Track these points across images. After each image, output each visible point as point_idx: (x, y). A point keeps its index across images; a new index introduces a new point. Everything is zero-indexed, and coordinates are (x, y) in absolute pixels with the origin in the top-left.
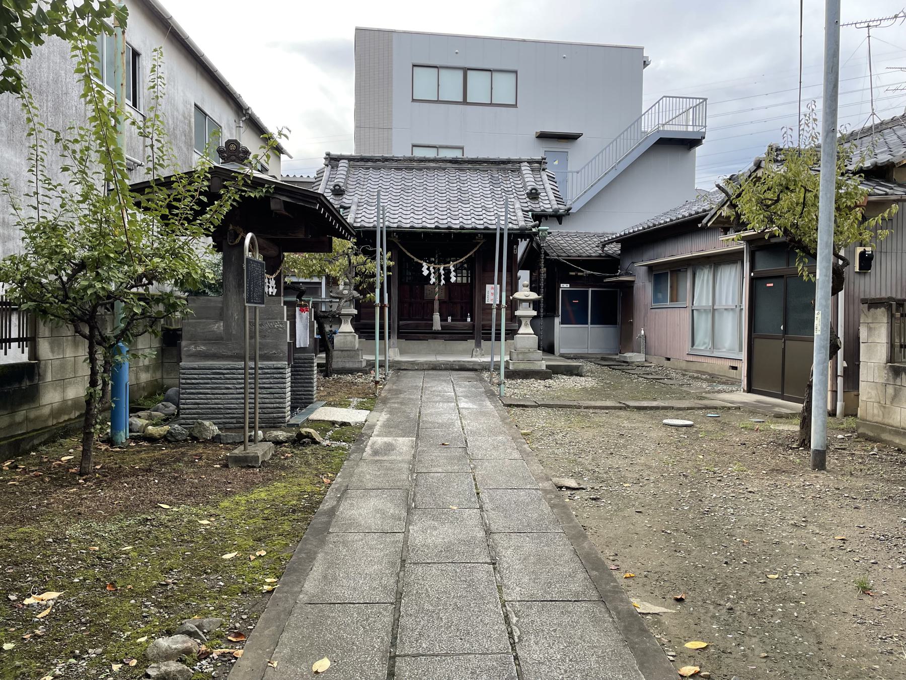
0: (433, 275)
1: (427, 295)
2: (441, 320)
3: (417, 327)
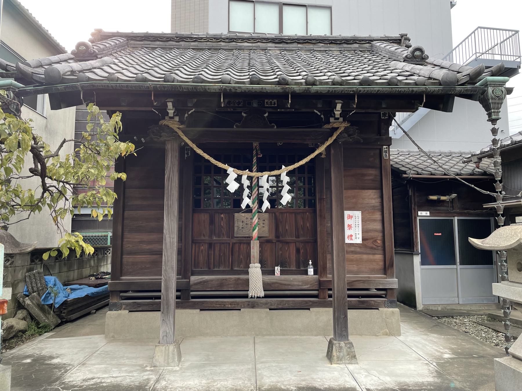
0: (247, 191)
2: (264, 273)
3: (221, 285)
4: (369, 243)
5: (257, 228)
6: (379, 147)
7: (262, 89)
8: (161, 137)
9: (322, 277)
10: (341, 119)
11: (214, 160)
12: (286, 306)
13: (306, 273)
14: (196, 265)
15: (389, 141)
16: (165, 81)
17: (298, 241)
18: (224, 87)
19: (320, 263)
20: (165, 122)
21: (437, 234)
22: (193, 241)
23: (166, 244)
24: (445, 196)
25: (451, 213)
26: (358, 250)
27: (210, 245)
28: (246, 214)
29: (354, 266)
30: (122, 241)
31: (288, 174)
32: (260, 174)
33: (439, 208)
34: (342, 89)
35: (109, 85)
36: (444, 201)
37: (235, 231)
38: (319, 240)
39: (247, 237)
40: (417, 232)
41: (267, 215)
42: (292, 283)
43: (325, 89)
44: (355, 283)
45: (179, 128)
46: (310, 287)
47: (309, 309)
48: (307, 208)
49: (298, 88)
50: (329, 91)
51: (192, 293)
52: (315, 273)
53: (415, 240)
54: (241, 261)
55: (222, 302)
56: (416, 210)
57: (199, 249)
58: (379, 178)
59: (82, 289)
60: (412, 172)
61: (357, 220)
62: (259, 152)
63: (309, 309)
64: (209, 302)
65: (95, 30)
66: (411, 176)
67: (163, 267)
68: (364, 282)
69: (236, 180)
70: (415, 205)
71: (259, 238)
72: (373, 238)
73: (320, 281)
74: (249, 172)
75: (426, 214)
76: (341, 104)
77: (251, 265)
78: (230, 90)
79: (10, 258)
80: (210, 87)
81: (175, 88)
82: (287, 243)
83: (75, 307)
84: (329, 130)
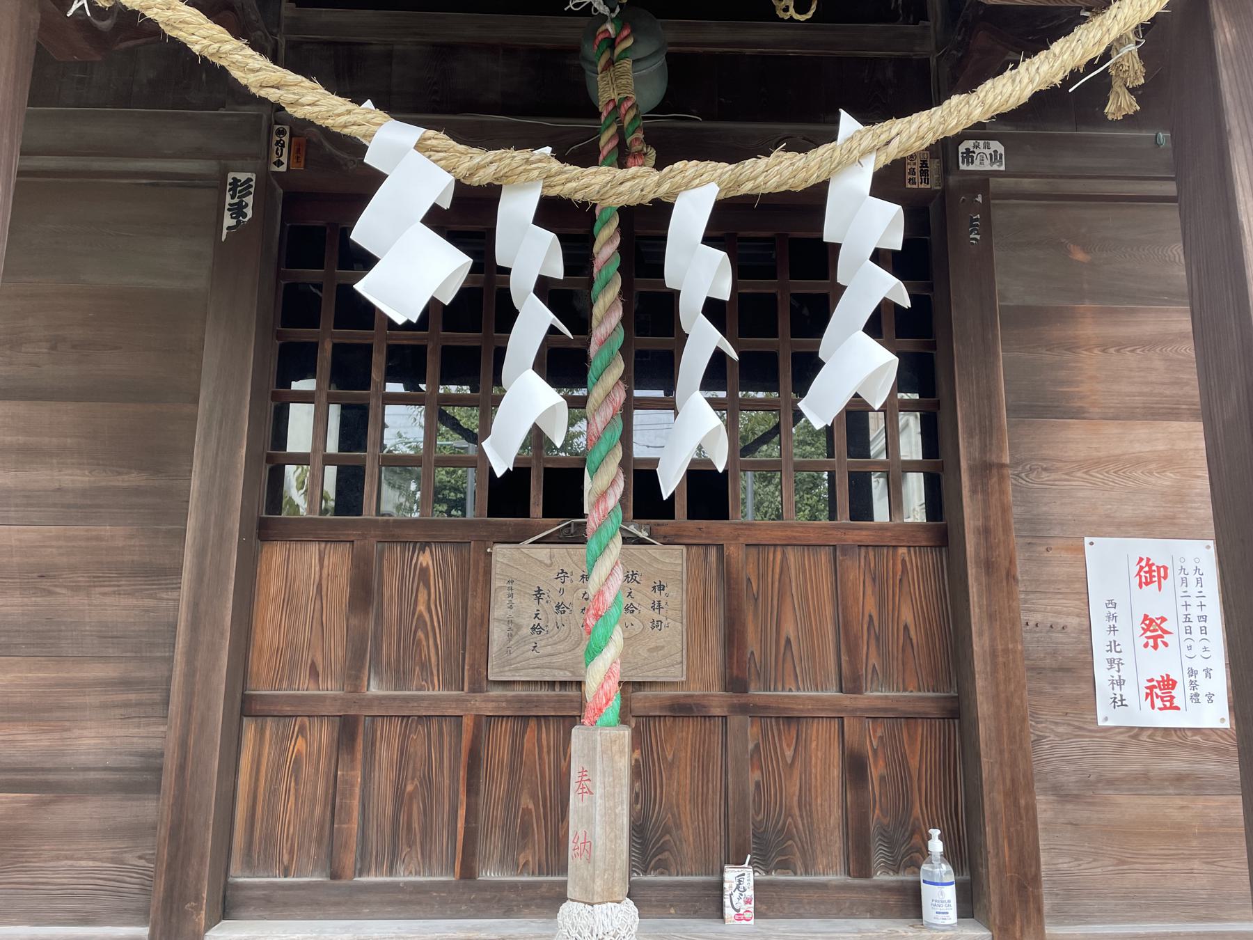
0: (534, 322)
17: (856, 713)
22: (246, 706)
27: (348, 730)
28: (559, 551)
29: (1196, 864)
37: (494, 649)
38: (984, 708)
39: (563, 684)
54: (526, 832)
61: (1193, 589)
69: (435, 219)
74: (556, 165)
82: (791, 720)
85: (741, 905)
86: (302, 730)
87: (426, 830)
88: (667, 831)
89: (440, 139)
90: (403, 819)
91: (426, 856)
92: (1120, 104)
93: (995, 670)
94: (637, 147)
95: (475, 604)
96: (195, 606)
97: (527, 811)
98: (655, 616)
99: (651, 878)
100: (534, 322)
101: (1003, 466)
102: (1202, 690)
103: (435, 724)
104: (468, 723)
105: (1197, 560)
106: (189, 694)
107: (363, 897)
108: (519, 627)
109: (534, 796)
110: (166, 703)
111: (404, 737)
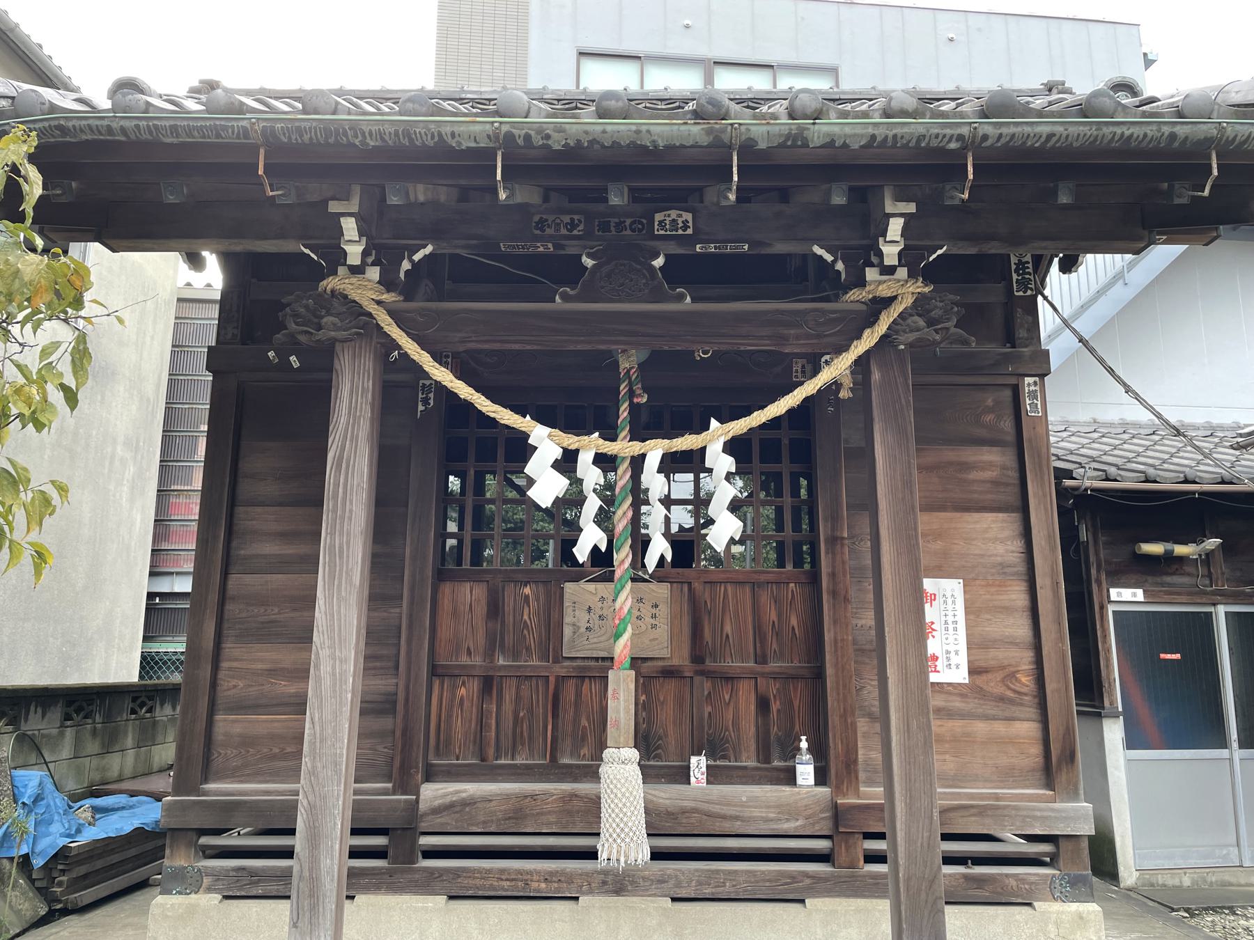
0: (592, 504)
1: (579, 638)
3: (516, 815)
4: (993, 684)
5: (629, 628)
6: (1013, 381)
7: (638, 132)
8: (319, 328)
9: (844, 795)
10: (902, 273)
11: (488, 403)
12: (727, 890)
13: (789, 777)
14: (443, 747)
15: (1040, 365)
16: (304, 111)
17: (763, 675)
18: (505, 128)
19: (836, 747)
20: (337, 282)
21: (1169, 656)
22: (435, 671)
23: (318, 680)
24: (1185, 543)
25: (1205, 593)
26: (957, 704)
27: (488, 684)
28: (600, 586)
29: (947, 757)
30: (216, 668)
31: (732, 447)
32: (636, 448)
33: (1168, 579)
34: (921, 130)
35: (114, 125)
36: (1182, 559)
37: (565, 639)
38: (830, 671)
39: (603, 659)
40: (1109, 650)
41: (661, 591)
42: (747, 813)
43: (859, 130)
44: (951, 815)
45: (379, 303)
46: (803, 826)
47: (802, 901)
48: (789, 567)
49: (765, 128)
50: (873, 137)
51: (425, 841)
52: (821, 777)
53: (1104, 673)
54: (584, 738)
55: (519, 872)
56: (1104, 585)
57: (454, 695)
58: (1014, 475)
59: (131, 807)
60: (1091, 473)
61: (950, 607)
62: (638, 388)
63: (802, 901)
64: (479, 871)
65: (201, 82)
66: (1087, 483)
67: (306, 760)
68: (982, 811)
69: (557, 465)
70: (1098, 571)
71: (636, 662)
72: (1003, 668)
73: (835, 807)
74: (601, 441)
75: (1134, 595)
76: (901, 221)
77: (607, 753)
78: (527, 137)
79: (85, 704)
80: (457, 129)
81: (337, 131)
82: (729, 679)
83: (99, 864)
84: (864, 307)
85: (699, 775)
86: (464, 683)
87: (531, 738)
88: (660, 738)
89: (556, 432)
90: (518, 730)
91: (531, 750)
92: (844, 394)
93: (836, 651)
94: (638, 392)
95: (554, 615)
96: (410, 616)
97: (585, 727)
98: (653, 621)
99: (651, 763)
100: (592, 504)
101: (843, 538)
102: (953, 662)
103: (534, 680)
104: (552, 680)
105: (953, 590)
106: (409, 663)
107: (499, 771)
108: (579, 628)
109: (588, 719)
110: (397, 667)
111: (518, 688)
